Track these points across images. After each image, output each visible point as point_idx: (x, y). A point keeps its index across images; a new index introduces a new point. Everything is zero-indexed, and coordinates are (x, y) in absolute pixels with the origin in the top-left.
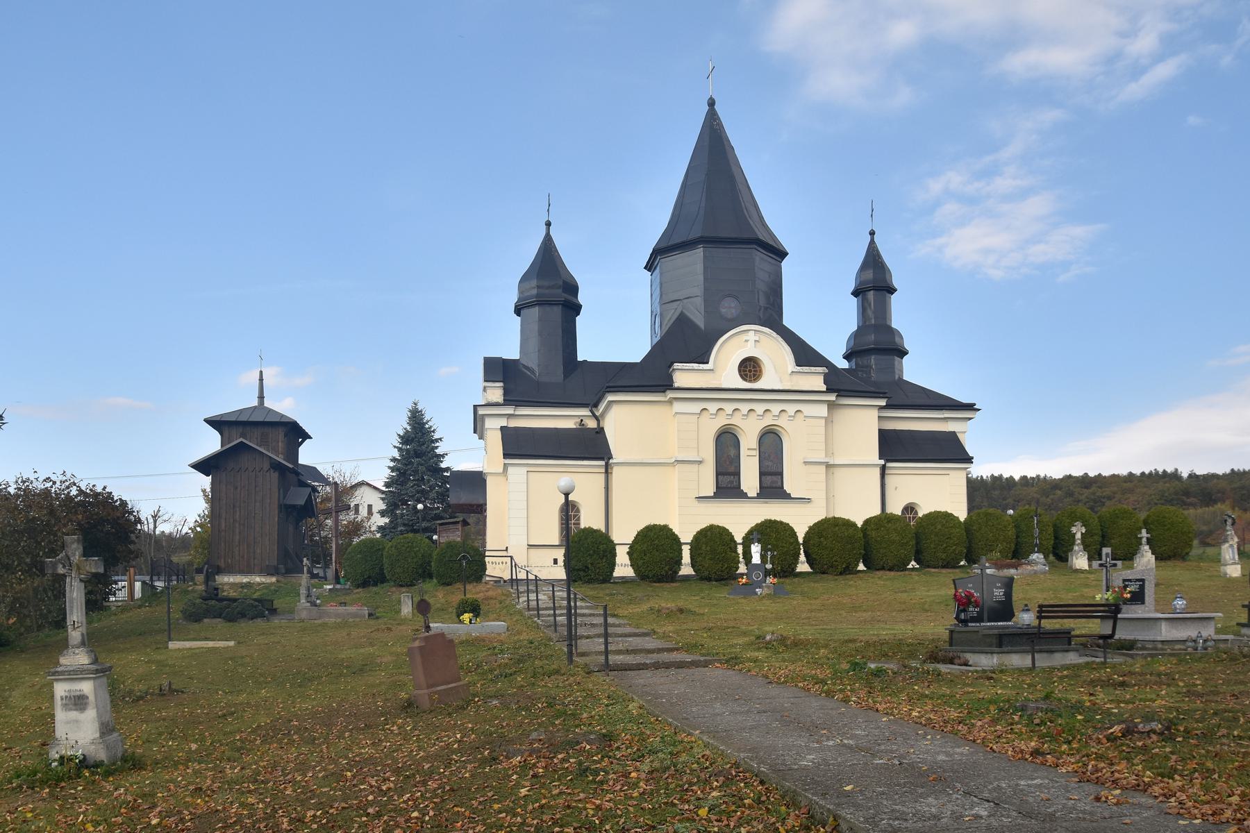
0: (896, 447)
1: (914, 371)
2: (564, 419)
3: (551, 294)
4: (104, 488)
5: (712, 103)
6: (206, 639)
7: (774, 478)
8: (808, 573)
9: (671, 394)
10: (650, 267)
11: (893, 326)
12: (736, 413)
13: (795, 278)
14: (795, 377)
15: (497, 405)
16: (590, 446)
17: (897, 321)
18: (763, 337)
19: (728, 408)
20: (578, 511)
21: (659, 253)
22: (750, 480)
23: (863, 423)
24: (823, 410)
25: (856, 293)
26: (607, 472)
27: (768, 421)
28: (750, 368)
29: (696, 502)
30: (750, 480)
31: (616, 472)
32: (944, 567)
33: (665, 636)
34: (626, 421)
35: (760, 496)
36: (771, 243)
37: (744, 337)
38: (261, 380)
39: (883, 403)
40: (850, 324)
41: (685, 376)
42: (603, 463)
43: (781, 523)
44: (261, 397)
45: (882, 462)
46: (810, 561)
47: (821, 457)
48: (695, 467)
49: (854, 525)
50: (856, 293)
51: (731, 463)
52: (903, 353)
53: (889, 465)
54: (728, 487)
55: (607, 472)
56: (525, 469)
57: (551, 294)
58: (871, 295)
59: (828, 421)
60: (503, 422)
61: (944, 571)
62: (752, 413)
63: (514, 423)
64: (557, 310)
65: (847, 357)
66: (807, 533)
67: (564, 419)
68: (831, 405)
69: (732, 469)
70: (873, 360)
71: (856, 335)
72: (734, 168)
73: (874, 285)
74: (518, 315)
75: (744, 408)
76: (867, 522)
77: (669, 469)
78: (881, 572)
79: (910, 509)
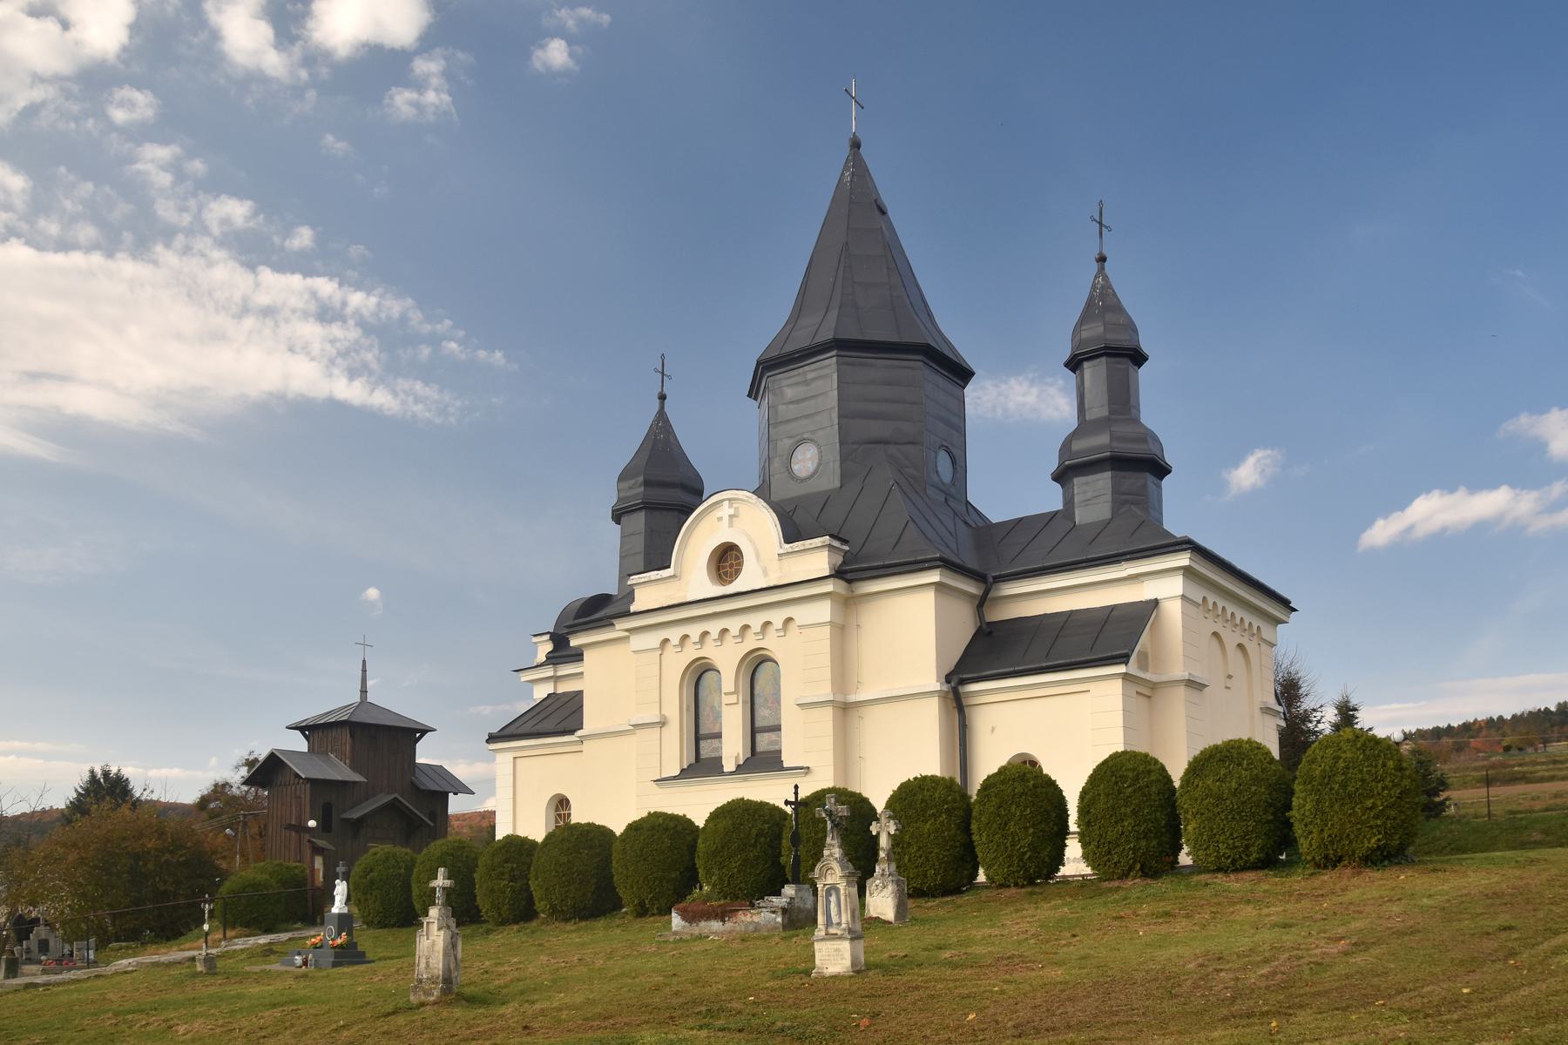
0: (994, 651)
4: (1266, 710)
5: (856, 145)
6: (156, 964)
9: (621, 625)
10: (754, 392)
14: (787, 562)
21: (769, 366)
22: (732, 748)
28: (726, 559)
30: (732, 748)
33: (78, 990)
35: (741, 769)
37: (718, 513)
38: (364, 671)
44: (364, 691)
52: (1161, 470)
56: (509, 756)
68: (848, 604)
74: (618, 522)
75: (714, 627)
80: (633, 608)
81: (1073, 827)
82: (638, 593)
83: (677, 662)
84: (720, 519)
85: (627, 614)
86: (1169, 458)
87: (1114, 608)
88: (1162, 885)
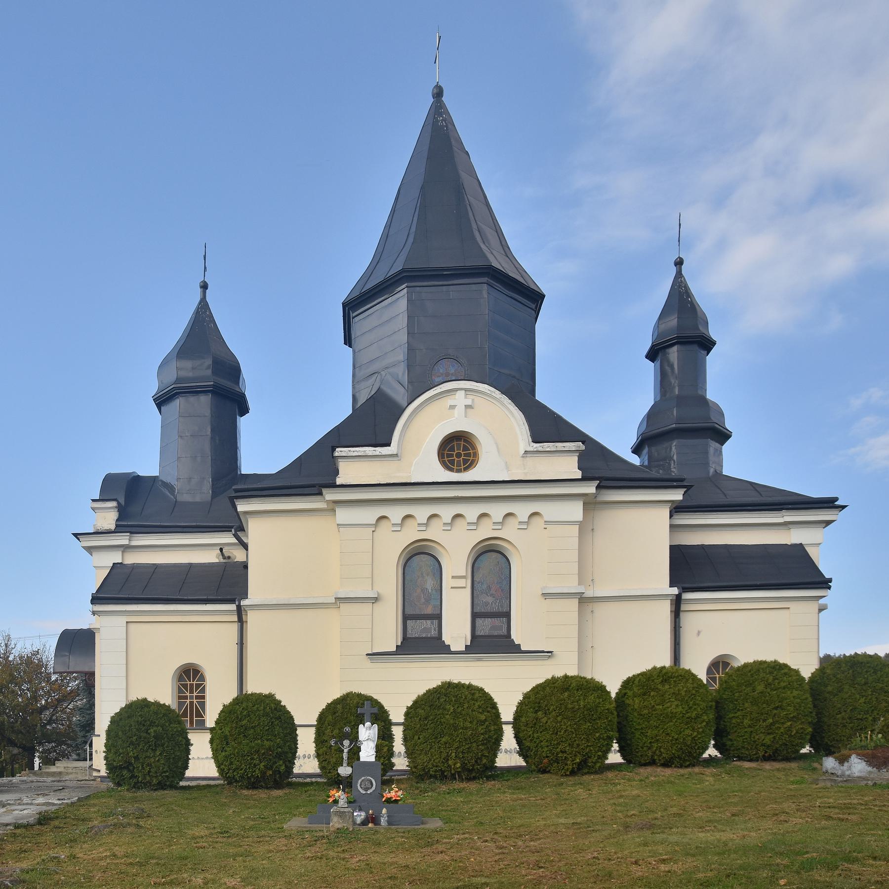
1: (737, 462)
2: (198, 550)
3: (208, 384)
5: (438, 93)
7: (497, 621)
8: (621, 764)
9: (330, 495)
11: (710, 396)
12: (435, 521)
13: (551, 333)
14: (531, 461)
15: (109, 532)
16: (225, 585)
17: (715, 390)
18: (479, 401)
19: (422, 513)
20: (202, 678)
22: (456, 628)
23: (645, 531)
24: (576, 511)
25: (652, 355)
26: (241, 621)
27: (486, 531)
28: (457, 449)
29: (367, 662)
30: (456, 628)
31: (252, 617)
32: (766, 759)
34: (277, 544)
35: (469, 650)
36: (513, 274)
37: (449, 401)
39: (677, 495)
40: (644, 398)
41: (355, 467)
42: (233, 607)
43: (470, 687)
45: (675, 591)
46: (622, 751)
47: (572, 586)
48: (367, 607)
49: (600, 689)
50: (652, 355)
51: (428, 601)
52: (723, 436)
53: (687, 596)
54: (420, 639)
55: (241, 621)
56: (123, 620)
57: (208, 384)
58: (674, 353)
59: (585, 528)
60: (116, 557)
61: (768, 766)
62: (459, 521)
63: (132, 559)
64: (204, 402)
65: (637, 450)
66: (521, 705)
67: (198, 550)
68: (590, 504)
69: (429, 610)
70: (674, 447)
71: (652, 416)
72: (464, 175)
73: (683, 337)
75: (447, 512)
76: (628, 684)
77: (332, 613)
78: (649, 769)
79: (719, 664)
80: (339, 481)
81: (508, 732)
82: (342, 466)
83: (393, 544)
84: (452, 407)
85: (333, 486)
86: (729, 425)
87: (191, 565)
88: (169, 795)
